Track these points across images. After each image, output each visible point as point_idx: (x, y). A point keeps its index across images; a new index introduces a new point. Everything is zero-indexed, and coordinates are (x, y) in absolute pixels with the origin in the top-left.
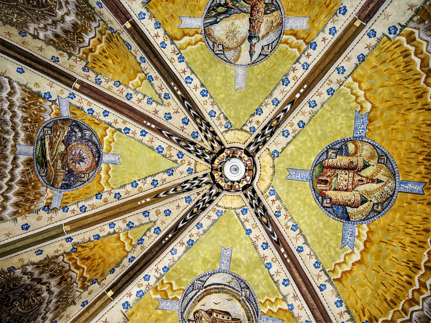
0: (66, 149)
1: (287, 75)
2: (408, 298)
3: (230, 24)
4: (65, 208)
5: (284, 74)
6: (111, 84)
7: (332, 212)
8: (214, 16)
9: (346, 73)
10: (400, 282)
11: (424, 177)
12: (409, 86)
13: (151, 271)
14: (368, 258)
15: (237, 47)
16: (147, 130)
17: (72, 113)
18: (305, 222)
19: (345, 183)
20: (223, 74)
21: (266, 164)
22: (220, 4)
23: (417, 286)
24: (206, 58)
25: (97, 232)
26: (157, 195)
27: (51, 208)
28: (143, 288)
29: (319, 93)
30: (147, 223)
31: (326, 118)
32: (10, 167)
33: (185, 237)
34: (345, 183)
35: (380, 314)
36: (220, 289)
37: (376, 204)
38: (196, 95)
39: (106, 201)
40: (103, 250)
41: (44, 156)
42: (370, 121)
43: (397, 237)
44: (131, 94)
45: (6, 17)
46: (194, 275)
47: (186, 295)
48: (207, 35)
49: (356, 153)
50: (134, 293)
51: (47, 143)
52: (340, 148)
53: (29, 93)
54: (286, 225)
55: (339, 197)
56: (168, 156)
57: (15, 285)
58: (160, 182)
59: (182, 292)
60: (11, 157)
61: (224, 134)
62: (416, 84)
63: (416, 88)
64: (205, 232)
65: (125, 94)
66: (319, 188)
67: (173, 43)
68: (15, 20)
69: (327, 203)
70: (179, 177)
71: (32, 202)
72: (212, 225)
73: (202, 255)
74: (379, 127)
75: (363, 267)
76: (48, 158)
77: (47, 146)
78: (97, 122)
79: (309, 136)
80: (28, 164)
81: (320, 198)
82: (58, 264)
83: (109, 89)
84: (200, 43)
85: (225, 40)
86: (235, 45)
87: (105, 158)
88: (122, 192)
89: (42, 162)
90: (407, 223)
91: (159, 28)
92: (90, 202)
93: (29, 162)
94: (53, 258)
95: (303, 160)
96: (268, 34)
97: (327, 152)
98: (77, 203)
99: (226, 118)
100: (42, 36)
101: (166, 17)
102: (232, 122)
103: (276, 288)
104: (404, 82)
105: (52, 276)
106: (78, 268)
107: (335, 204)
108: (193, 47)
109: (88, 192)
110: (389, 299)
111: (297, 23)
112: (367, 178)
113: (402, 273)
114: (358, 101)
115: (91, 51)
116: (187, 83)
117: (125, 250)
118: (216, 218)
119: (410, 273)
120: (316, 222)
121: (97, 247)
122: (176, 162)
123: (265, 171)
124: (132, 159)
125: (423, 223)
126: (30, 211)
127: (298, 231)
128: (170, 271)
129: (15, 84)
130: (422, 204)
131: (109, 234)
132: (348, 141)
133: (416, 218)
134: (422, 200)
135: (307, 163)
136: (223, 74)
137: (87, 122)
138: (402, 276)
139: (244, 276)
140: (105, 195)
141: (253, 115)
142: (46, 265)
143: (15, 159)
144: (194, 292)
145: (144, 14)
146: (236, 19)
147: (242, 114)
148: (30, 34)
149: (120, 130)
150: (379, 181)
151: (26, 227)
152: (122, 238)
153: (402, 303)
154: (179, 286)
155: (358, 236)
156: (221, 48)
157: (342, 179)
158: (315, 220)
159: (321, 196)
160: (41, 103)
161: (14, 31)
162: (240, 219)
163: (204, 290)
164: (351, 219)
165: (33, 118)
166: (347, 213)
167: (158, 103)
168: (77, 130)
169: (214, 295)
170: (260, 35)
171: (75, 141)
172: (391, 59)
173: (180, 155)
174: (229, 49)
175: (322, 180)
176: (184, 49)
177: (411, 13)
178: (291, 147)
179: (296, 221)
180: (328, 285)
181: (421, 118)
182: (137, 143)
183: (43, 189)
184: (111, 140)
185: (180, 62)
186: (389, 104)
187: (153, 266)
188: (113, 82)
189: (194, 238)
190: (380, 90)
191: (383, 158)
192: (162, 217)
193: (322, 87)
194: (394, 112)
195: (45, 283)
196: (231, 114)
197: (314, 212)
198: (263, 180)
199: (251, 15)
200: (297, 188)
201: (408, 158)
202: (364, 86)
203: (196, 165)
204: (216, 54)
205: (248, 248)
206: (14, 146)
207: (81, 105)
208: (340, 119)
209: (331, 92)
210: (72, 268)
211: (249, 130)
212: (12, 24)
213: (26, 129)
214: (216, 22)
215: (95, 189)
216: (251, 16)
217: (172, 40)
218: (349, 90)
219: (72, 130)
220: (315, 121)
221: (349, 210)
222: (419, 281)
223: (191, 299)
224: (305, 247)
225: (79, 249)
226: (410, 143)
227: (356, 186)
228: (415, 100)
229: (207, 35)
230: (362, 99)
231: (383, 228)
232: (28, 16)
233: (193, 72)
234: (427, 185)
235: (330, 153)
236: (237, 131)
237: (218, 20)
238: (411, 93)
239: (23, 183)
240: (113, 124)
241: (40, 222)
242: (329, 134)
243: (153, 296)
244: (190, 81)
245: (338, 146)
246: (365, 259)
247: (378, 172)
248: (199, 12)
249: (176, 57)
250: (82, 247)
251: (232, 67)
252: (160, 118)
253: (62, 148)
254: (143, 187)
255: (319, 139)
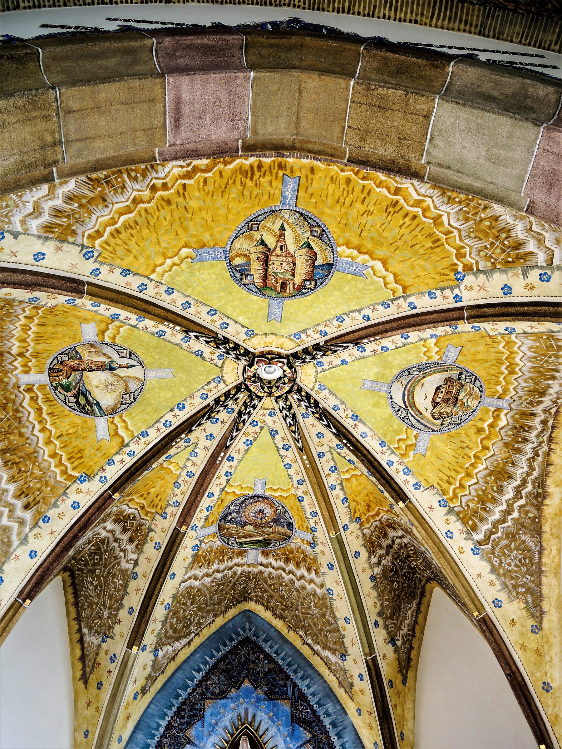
0: (250, 524)
1: (153, 334)
2: (433, 225)
3: (97, 389)
4: (313, 530)
5: (151, 336)
6: (177, 491)
7: (321, 280)
8: (91, 406)
9: (145, 281)
10: (412, 227)
11: (276, 177)
12: (156, 217)
13: (383, 460)
14: (381, 252)
15: (124, 381)
16: (227, 456)
17: (212, 524)
18: (333, 308)
19: (284, 264)
20: (157, 390)
21: (263, 342)
22: (76, 402)
23: (419, 211)
24: (141, 410)
25: (339, 502)
26: (300, 448)
27: (312, 541)
28: (401, 468)
29: (174, 303)
30: (332, 454)
31: (203, 290)
32: (271, 569)
33: (348, 423)
34: (284, 264)
35: (447, 259)
36: (409, 394)
37: (311, 232)
38: (183, 415)
39: (306, 493)
40: (360, 493)
41: (259, 541)
42: (204, 246)
43: (355, 217)
44: (188, 472)
45: (119, 590)
46: (392, 417)
47: (413, 426)
48: (113, 411)
49: (246, 255)
50: (405, 477)
51: (244, 540)
52: (240, 274)
53: (194, 563)
54: (336, 327)
55: (303, 272)
56: (255, 436)
57: (392, 570)
58: (285, 442)
59: (409, 430)
60: (261, 568)
61: (227, 383)
62: (152, 211)
63: (158, 209)
64: (343, 403)
65: (187, 478)
66: (291, 291)
67: (128, 445)
68: (121, 582)
69: (310, 284)
70: (279, 424)
71: (306, 556)
72: (335, 396)
73: (369, 408)
74: (211, 235)
75: (390, 261)
76: (261, 538)
77: (248, 539)
78: (220, 502)
79: (226, 304)
80: (268, 555)
81: (303, 291)
82: (372, 532)
83: (184, 494)
84: (124, 418)
85: (117, 392)
86: (121, 383)
87: (259, 491)
88: (296, 478)
89: (266, 543)
90: (338, 202)
91: (113, 460)
92: (307, 507)
93: (266, 554)
94: (365, 539)
95: (256, 307)
96: (104, 354)
97: (245, 285)
98: (308, 519)
99: (209, 383)
100: (134, 557)
101: (100, 455)
102: (213, 377)
103: (410, 345)
104: (152, 223)
105: (386, 535)
106: (378, 514)
107: (312, 277)
108: (129, 424)
109: (296, 508)
110: (431, 245)
111: (89, 332)
112: (278, 241)
113: (401, 222)
114: (179, 262)
115: (143, 508)
116: (171, 425)
117: (361, 475)
118: (327, 391)
119: (402, 213)
120: (334, 298)
121: (356, 499)
122: (261, 428)
123: (271, 343)
124: (261, 465)
125: (338, 183)
126: (315, 560)
127: (345, 317)
128: (385, 440)
129: (186, 577)
130: (312, 180)
131: (342, 489)
132: (231, 265)
133: (331, 191)
134: (307, 180)
135: (260, 303)
136: (157, 390)
137: (221, 510)
138: (404, 223)
139: (396, 372)
140: (300, 493)
141: (204, 359)
142: (371, 545)
143: (261, 565)
144: (410, 418)
145: (101, 477)
146: (91, 384)
147: (203, 368)
148: (134, 568)
149: (228, 481)
150: (282, 228)
151: (331, 566)
152: (348, 476)
153: (437, 232)
154: (402, 432)
155: (352, 258)
156: (127, 396)
157: (279, 268)
158: (331, 298)
159: (300, 290)
160: (203, 552)
161: (133, 585)
162: (329, 369)
163: (409, 408)
164: (331, 262)
165: (219, 555)
166: (323, 265)
167: (196, 447)
168: (230, 517)
169: (416, 399)
170: (107, 360)
171: (242, 517)
172: (124, 245)
173: (254, 424)
174: (127, 388)
175: (281, 287)
176: (133, 432)
177: (66, 247)
178: (241, 319)
179: (332, 317)
180: (410, 300)
181: (197, 194)
182: (242, 464)
183: (292, 545)
184: (239, 487)
185: (148, 435)
186: (180, 231)
187: (378, 457)
188: (175, 489)
189: (350, 414)
190: (163, 244)
191: (252, 225)
192: (325, 440)
193: (165, 301)
194: (190, 224)
195: (393, 541)
196: (204, 379)
197: (322, 298)
198: (282, 344)
199: (82, 370)
200: (291, 313)
201: (251, 199)
202: (160, 260)
203: (265, 409)
204: (135, 399)
205: (363, 365)
206: (249, 565)
207: (203, 518)
208: (203, 276)
209: (170, 291)
210: (378, 518)
211: (222, 361)
212: (126, 586)
213: (231, 558)
214: (98, 404)
215: (293, 501)
216: (85, 370)
217: (124, 446)
218: (166, 275)
219: (229, 521)
220: (207, 300)
221: (319, 262)
222: (412, 206)
223: (418, 421)
224: (364, 312)
225: (357, 515)
226: (230, 198)
227: (289, 254)
228: (174, 206)
229: (113, 411)
230: (176, 260)
231: (343, 231)
232: (113, 566)
233: (158, 421)
234: (288, 172)
235: (247, 282)
236: (223, 372)
237: (95, 402)
238: (165, 212)
239: (287, 560)
240: (222, 487)
241: (326, 553)
242: (223, 285)
243: (411, 459)
244: (168, 423)
245: (238, 275)
246: (380, 257)
247: (269, 229)
248: (89, 422)
249: (143, 440)
250: (355, 512)
251: (148, 383)
252: (213, 445)
253: (249, 528)
254: (291, 458)
255: (230, 293)
